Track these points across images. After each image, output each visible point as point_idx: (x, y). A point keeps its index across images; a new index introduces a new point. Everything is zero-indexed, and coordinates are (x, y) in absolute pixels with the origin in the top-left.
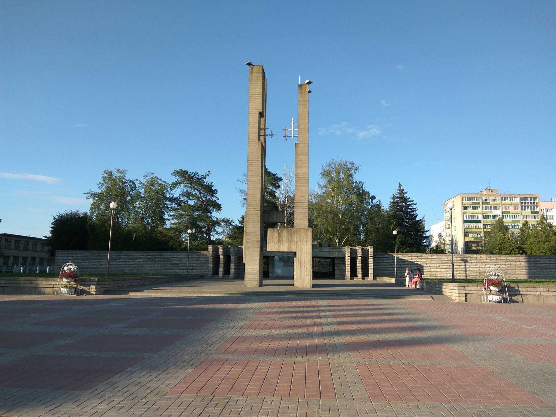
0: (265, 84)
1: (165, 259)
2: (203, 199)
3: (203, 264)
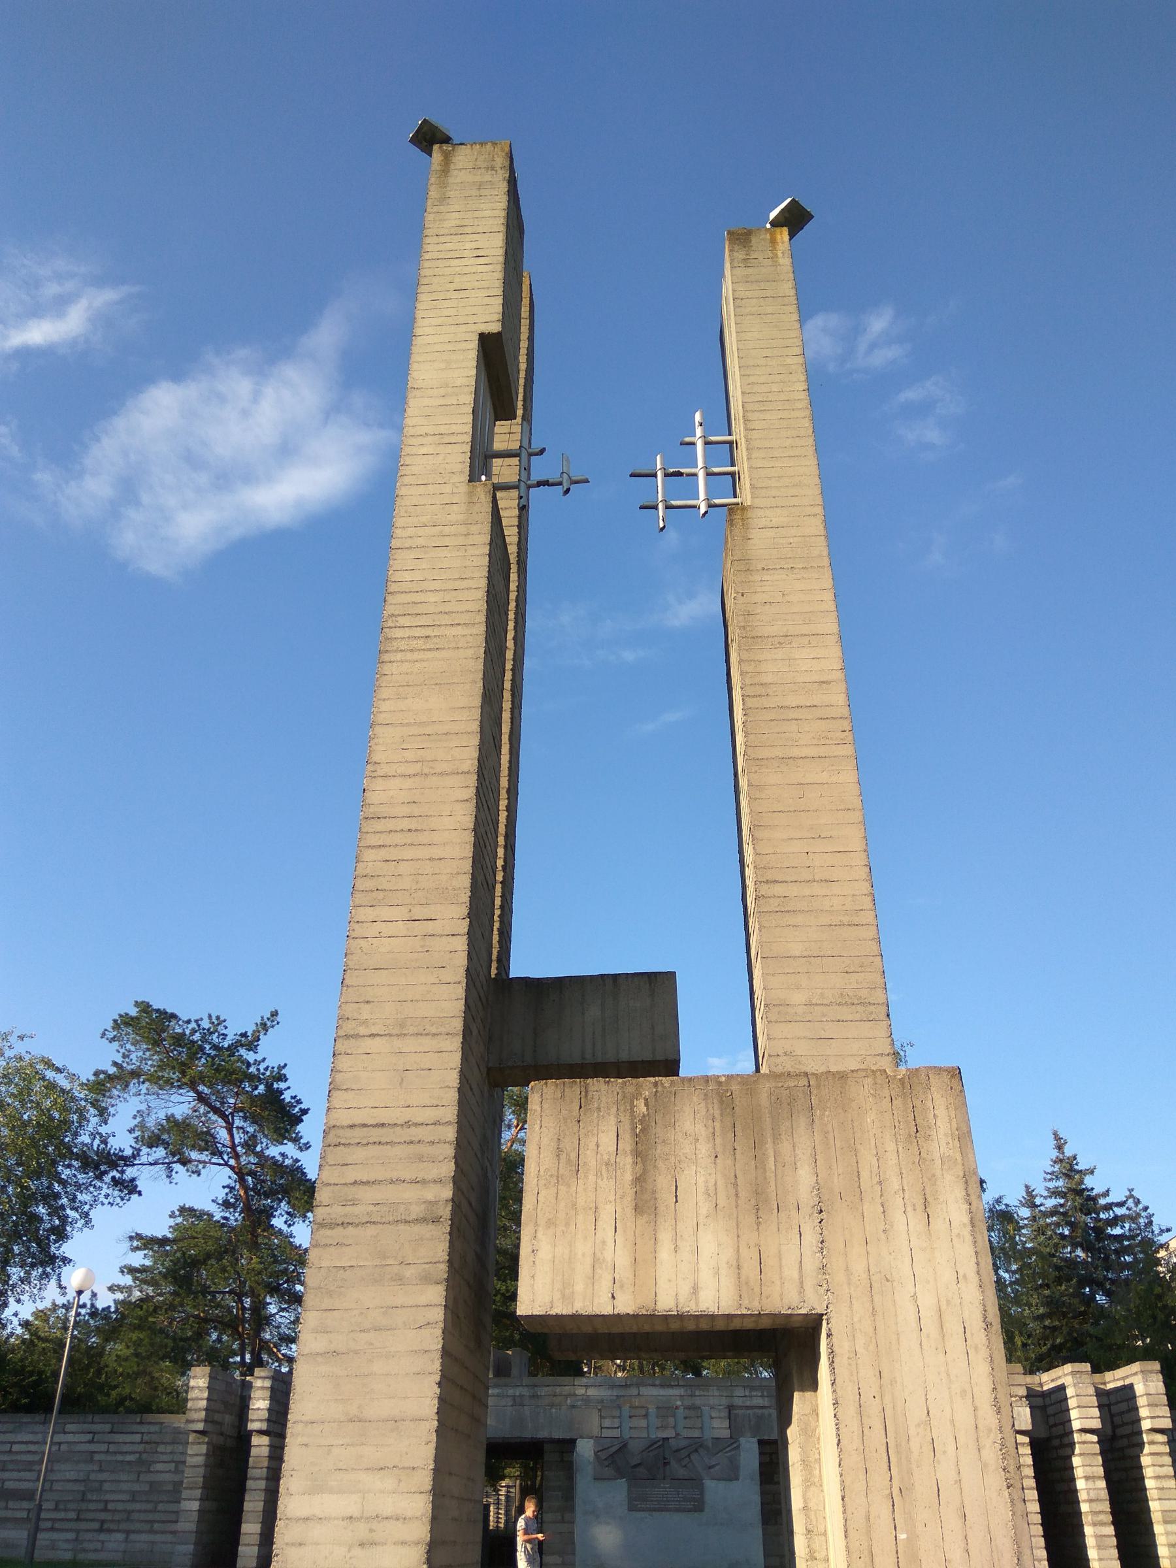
0: (525, 311)
2: (244, 1160)
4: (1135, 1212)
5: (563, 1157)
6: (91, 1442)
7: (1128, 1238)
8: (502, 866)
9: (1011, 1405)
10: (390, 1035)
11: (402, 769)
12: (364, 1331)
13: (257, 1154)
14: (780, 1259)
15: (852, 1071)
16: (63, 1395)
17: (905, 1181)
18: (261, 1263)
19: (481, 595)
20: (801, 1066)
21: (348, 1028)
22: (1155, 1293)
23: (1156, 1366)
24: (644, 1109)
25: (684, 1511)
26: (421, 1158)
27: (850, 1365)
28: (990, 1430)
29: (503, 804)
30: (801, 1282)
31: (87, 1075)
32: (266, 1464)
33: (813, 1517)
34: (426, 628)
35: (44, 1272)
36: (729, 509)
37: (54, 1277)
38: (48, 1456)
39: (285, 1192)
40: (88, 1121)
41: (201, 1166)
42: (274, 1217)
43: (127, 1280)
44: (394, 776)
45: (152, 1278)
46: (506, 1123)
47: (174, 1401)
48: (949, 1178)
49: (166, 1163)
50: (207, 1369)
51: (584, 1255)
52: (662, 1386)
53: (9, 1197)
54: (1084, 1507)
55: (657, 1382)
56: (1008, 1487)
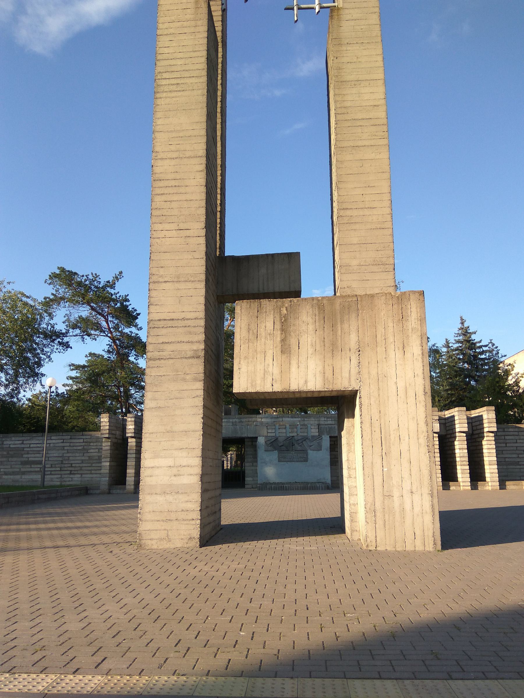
1: (11, 453)
2: (114, 334)
3: (95, 462)
4: (492, 349)
5: (251, 332)
6: (63, 442)
7: (487, 359)
8: (220, 203)
9: (432, 423)
10: (173, 282)
11: (170, 155)
12: (171, 399)
13: (119, 332)
14: (341, 370)
15: (377, 294)
16: (49, 426)
17: (396, 338)
18: (126, 374)
19: (204, 60)
20: (354, 292)
21: (154, 278)
22: (496, 380)
23: (493, 408)
24: (285, 312)
25: (300, 461)
26: (190, 333)
27: (368, 408)
28: (423, 432)
29: (219, 172)
30: (350, 378)
31: (41, 299)
32: (135, 448)
33: (350, 463)
34: (177, 79)
35: (34, 380)
36: (331, 9)
37: (39, 381)
38: (46, 448)
39: (133, 347)
40: (44, 318)
41: (96, 337)
42: (130, 356)
43: (70, 382)
44: (166, 159)
45: (81, 381)
46: (226, 318)
47: (95, 427)
48: (414, 336)
49: (81, 335)
50: (108, 415)
51: (260, 370)
52: (292, 417)
53: (14, 350)
54: (458, 459)
55: (290, 416)
56: (429, 452)
